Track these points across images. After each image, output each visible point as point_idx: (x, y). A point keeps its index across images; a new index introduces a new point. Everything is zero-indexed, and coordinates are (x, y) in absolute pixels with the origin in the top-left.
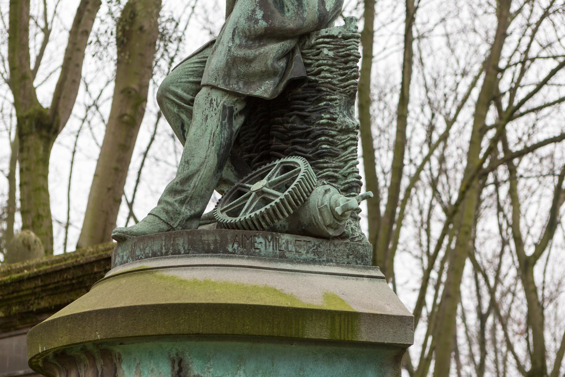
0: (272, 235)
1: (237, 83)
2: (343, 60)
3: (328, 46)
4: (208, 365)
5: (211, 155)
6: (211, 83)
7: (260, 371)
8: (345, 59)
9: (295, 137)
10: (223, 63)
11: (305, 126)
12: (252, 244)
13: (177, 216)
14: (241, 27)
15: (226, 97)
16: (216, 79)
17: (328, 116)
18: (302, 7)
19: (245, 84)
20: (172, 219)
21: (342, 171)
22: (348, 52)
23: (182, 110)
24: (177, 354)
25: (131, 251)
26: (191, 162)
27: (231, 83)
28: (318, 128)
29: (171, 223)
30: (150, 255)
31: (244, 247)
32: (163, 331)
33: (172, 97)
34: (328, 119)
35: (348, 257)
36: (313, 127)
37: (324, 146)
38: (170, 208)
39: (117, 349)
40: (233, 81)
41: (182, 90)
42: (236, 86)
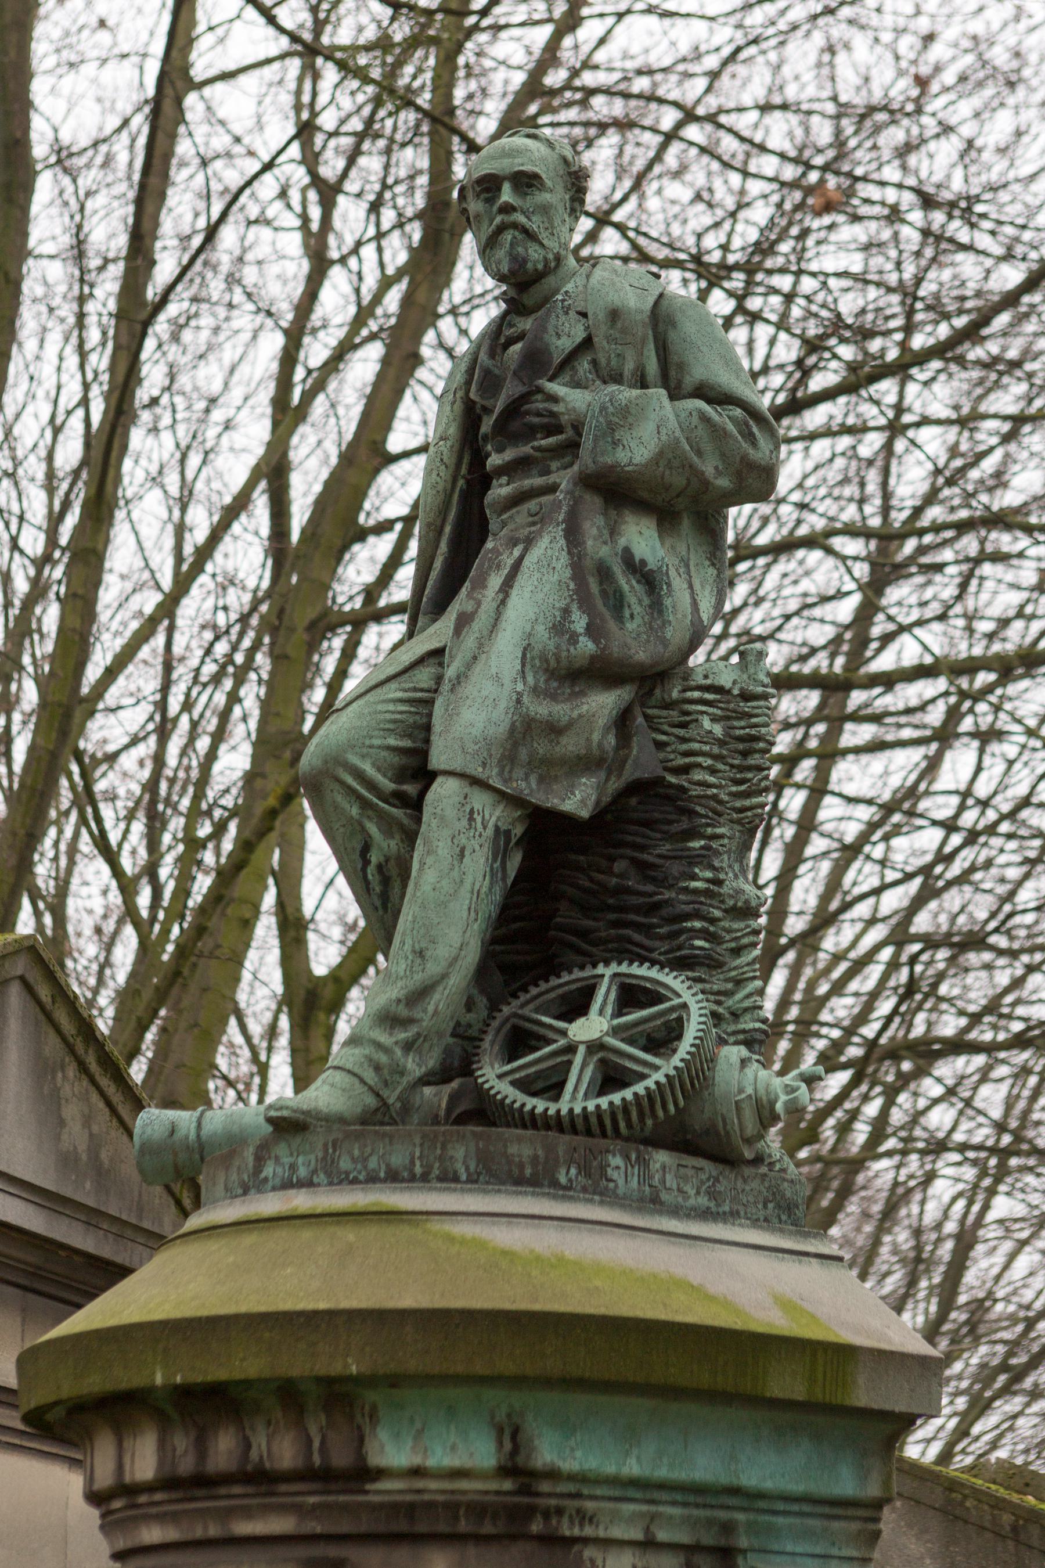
0: (638, 1152)
1: (526, 778)
2: (741, 746)
3: (711, 710)
4: (572, 1443)
5: (472, 942)
6: (474, 773)
7: (665, 1460)
8: (747, 745)
9: (622, 909)
10: (503, 728)
11: (649, 888)
12: (603, 1168)
13: (396, 1077)
14: (538, 647)
15: (501, 807)
16: (484, 765)
17: (709, 874)
18: (661, 612)
19: (541, 780)
20: (386, 1084)
21: (730, 1002)
22: (753, 732)
23: (370, 813)
24: (509, 1416)
25: (324, 1159)
26: (428, 954)
27: (515, 776)
28: (681, 897)
29: (385, 1093)
30: (382, 1175)
31: (588, 1175)
32: (506, 1366)
33: (350, 780)
34: (708, 881)
35: (765, 1206)
36: (667, 895)
37: (698, 943)
38: (383, 1059)
39: (372, 1396)
40: (519, 773)
41: (373, 765)
42: (523, 785)
